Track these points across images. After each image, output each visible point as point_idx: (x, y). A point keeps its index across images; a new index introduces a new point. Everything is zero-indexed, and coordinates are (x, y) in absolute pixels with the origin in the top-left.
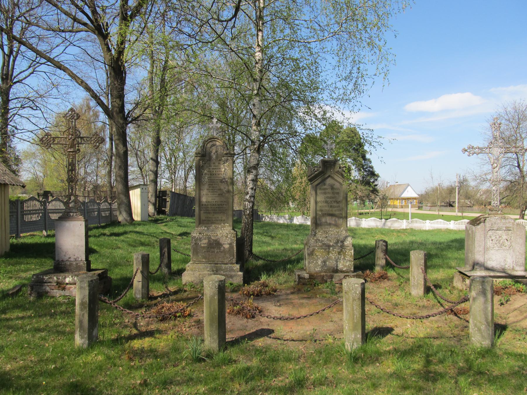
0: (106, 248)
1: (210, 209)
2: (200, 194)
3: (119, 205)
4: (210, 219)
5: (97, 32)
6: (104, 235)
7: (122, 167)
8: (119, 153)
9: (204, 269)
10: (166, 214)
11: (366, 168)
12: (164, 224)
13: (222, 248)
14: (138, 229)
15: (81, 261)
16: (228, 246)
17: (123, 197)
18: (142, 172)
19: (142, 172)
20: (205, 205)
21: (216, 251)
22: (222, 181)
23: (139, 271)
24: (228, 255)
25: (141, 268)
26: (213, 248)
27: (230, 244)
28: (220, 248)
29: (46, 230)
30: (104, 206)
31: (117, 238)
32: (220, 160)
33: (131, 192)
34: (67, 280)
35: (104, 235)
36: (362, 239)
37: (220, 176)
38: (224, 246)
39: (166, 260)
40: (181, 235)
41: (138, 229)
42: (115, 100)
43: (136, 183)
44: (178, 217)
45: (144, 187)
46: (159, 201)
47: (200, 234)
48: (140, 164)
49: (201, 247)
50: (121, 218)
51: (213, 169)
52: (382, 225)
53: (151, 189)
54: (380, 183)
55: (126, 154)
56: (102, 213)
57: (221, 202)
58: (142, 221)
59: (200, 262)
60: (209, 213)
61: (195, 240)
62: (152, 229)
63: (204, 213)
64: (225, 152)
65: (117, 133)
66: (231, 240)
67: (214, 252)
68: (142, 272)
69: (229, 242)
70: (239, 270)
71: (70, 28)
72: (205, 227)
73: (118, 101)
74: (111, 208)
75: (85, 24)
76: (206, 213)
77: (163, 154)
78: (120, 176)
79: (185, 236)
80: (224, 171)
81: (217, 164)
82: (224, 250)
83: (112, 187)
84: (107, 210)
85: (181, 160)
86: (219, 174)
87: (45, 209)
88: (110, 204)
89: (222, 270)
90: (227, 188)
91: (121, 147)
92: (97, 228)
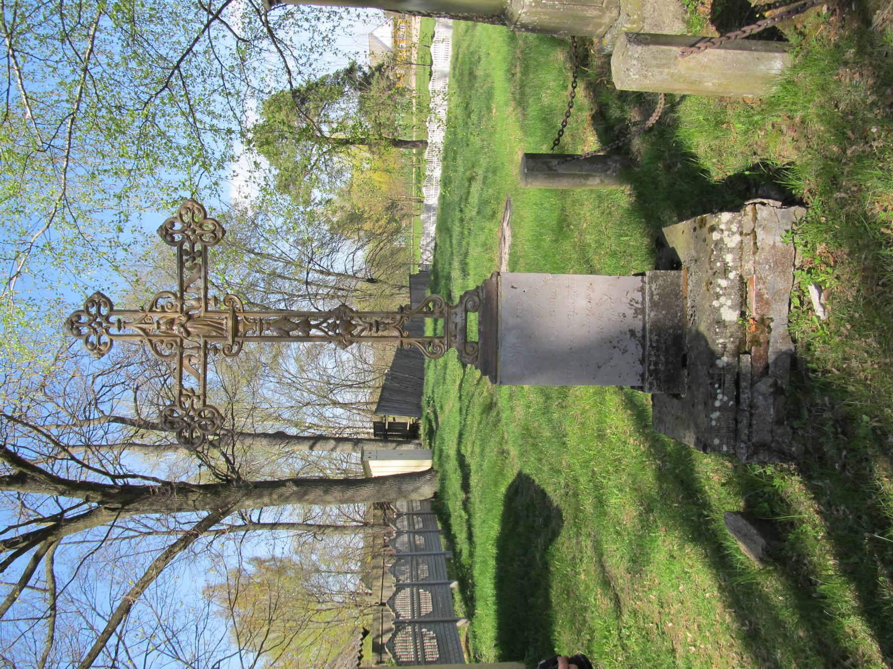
6: (466, 504)
15: (642, 290)
29: (456, 621)
30: (403, 524)
34: (730, 315)
42: (190, 502)
50: (427, 491)
54: (365, 62)
56: (416, 527)
71: (48, 595)
73: (193, 497)
75: (37, 559)
87: (412, 623)
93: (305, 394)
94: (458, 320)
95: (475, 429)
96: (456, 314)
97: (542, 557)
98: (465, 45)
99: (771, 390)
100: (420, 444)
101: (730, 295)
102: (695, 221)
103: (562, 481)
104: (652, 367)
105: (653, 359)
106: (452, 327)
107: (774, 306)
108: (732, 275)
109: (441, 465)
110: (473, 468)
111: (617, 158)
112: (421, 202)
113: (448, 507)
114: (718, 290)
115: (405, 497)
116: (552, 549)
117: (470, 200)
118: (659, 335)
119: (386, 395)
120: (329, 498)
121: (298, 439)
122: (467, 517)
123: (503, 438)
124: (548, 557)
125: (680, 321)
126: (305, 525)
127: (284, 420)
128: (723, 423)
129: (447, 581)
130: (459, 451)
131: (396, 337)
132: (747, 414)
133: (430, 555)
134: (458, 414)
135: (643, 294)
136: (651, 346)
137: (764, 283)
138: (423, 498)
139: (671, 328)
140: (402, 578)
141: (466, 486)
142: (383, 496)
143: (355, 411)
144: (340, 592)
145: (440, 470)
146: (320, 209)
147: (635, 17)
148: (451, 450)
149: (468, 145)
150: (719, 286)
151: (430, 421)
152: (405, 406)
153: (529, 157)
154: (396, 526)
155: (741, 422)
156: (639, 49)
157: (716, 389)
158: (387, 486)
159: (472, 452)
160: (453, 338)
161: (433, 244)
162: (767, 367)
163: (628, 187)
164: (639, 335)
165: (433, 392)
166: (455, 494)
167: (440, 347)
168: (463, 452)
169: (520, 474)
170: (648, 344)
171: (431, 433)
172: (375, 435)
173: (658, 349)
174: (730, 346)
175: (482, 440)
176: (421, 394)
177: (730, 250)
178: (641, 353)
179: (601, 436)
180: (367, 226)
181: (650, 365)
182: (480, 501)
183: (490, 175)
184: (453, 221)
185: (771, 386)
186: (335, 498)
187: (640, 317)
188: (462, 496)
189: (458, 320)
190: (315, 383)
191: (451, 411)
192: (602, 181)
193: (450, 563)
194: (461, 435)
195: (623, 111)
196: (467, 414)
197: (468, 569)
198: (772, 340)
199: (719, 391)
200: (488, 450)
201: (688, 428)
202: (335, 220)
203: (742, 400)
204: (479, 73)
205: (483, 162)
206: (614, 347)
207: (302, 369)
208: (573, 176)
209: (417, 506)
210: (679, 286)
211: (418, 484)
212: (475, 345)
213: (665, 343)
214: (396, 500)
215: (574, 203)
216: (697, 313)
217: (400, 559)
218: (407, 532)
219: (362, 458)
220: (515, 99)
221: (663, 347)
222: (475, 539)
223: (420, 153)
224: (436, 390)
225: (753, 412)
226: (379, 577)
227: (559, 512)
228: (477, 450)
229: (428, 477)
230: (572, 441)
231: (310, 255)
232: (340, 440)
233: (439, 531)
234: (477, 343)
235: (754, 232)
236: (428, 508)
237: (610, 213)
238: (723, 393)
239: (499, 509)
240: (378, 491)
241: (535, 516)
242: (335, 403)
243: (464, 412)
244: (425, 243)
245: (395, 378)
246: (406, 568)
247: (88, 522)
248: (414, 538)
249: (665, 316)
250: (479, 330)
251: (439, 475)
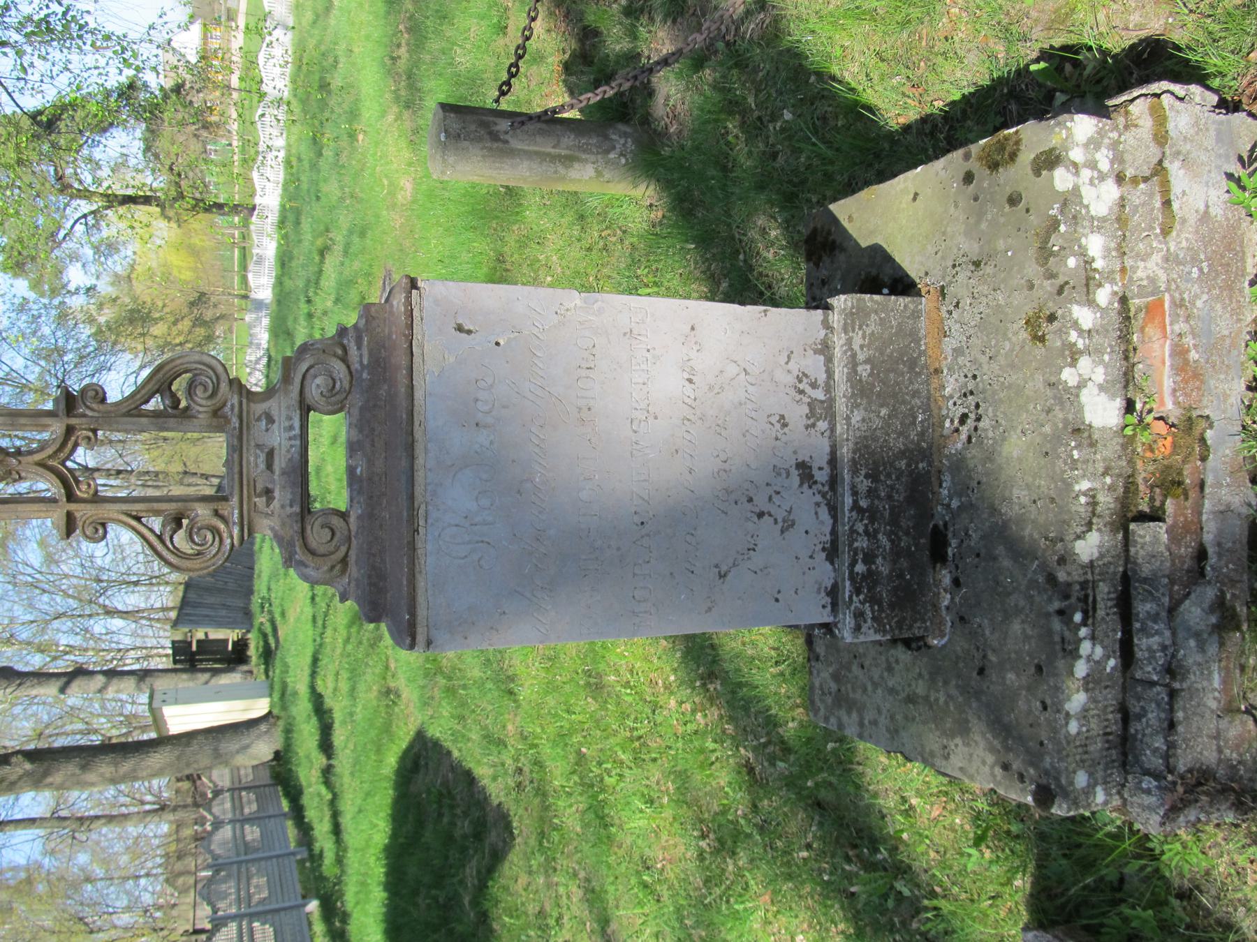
6: (327, 772)
15: (825, 349)
50: (263, 749)
56: (247, 811)
93: (58, 599)
94: (279, 438)
95: (339, 651)
96: (270, 420)
97: (475, 903)
98: (311, 43)
99: (1213, 619)
100: (251, 672)
101: (1099, 352)
102: (967, 157)
103: (509, 762)
104: (860, 568)
105: (862, 543)
106: (255, 462)
107: (1212, 383)
108: (1103, 296)
109: (284, 708)
110: (338, 716)
111: (622, 127)
112: (245, 297)
113: (298, 778)
114: (1073, 336)
115: (226, 763)
116: (494, 888)
117: (323, 283)
118: (873, 476)
119: (192, 596)
120: (91, 777)
121: (40, 676)
122: (329, 796)
123: (387, 667)
124: (487, 905)
125: (922, 434)
126: (56, 819)
127: (20, 643)
128: (1094, 724)
129: (300, 901)
130: (313, 688)
131: (53, 500)
132: (1160, 692)
133: (271, 858)
134: (309, 626)
135: (829, 360)
136: (856, 507)
137: (1188, 318)
138: (255, 762)
139: (902, 454)
140: (221, 905)
141: (326, 746)
142: (188, 765)
143: (144, 622)
144: (128, 909)
145: (282, 714)
146: (77, 302)
148: (299, 683)
149: (318, 198)
150: (1076, 325)
151: (265, 636)
152: (224, 613)
153: (445, 107)
154: (211, 813)
155: (1139, 717)
157: (1077, 627)
158: (195, 746)
159: (335, 689)
160: (260, 502)
161: (265, 360)
162: (1201, 554)
163: (651, 191)
164: (822, 476)
165: (269, 589)
166: (308, 757)
167: (215, 531)
168: (320, 688)
169: (420, 736)
170: (848, 501)
171: (268, 655)
172: (175, 662)
173: (872, 514)
174: (1106, 501)
175: (353, 671)
176: (250, 592)
177: (1098, 225)
178: (827, 529)
179: (596, 687)
180: (158, 330)
181: (853, 564)
182: (352, 774)
183: (356, 239)
184: (295, 320)
185: (1211, 610)
186: (102, 775)
187: (822, 425)
188: (321, 760)
189: (279, 438)
190: (75, 581)
191: (298, 620)
192: (599, 174)
193: (304, 867)
194: (315, 660)
195: (634, 36)
196: (324, 627)
197: (335, 884)
198: (1209, 480)
199: (1083, 632)
200: (361, 687)
201: (963, 729)
202: (102, 320)
203: (1139, 654)
204: (337, 81)
205: (344, 220)
206: (761, 515)
207: (50, 560)
208: (543, 157)
209: (248, 776)
210: (918, 341)
211: (246, 741)
212: (336, 522)
213: (890, 497)
214: (210, 768)
215: (522, 244)
216: (987, 410)
217: (217, 872)
218: (231, 821)
219: (150, 704)
220: (397, 99)
221: (885, 507)
222: (346, 837)
223: (246, 224)
224: (273, 586)
225: (1177, 685)
226: (189, 888)
227: (504, 820)
228: (344, 686)
229: (263, 727)
230: (526, 692)
231: (60, 375)
232: (112, 674)
233: (285, 815)
234: (343, 515)
235: (1159, 169)
236: (265, 776)
237: (605, 248)
238: (1093, 638)
239: (385, 796)
240: (178, 758)
241: (455, 815)
242: (110, 612)
243: (320, 623)
244: (253, 358)
246: (230, 887)
249: (887, 421)
250: (351, 471)
251: (281, 723)
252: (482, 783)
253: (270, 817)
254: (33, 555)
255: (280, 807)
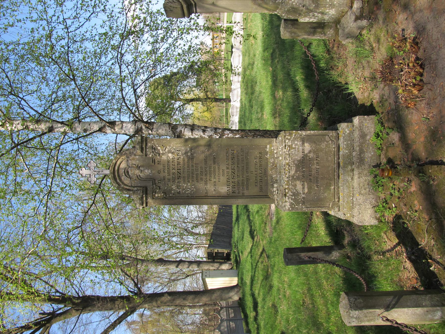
0: (275, 321)
1: (241, 178)
2: (214, 197)
3: (222, 300)
4: (259, 178)
5: (48, 325)
6: (256, 319)
7: (184, 297)
8: (170, 301)
9: (349, 187)
10: (230, 253)
11: (186, 73)
12: (240, 254)
13: (311, 155)
14: (248, 281)
16: (306, 145)
17: (214, 296)
18: (190, 275)
19: (190, 275)
20: (234, 187)
21: (315, 166)
22: (191, 158)
23: (385, 314)
24: (323, 145)
25: (378, 311)
26: (310, 171)
27: (303, 140)
28: (310, 160)
30: (224, 315)
31: (260, 305)
32: (154, 161)
33: (210, 287)
35: (256, 319)
36: (255, 56)
37: (181, 160)
38: (306, 152)
39: (320, 255)
40: (253, 237)
41: (248, 281)
42: (116, 306)
43: (201, 282)
44: (233, 240)
45: (204, 274)
46: (218, 259)
47: (285, 195)
48: (184, 277)
49: (309, 192)
51: (169, 173)
52: (238, 51)
53: (206, 267)
55: (170, 294)
56: (231, 316)
57: (227, 159)
58: (238, 276)
59: (337, 194)
60: (248, 180)
61: (298, 203)
62: (247, 266)
63: (247, 189)
64: (139, 152)
65: (150, 302)
66: (295, 139)
67: (317, 169)
68: (388, 308)
69: (299, 143)
70: (349, 124)
72: (273, 187)
73: (117, 303)
74: (225, 307)
76: (247, 184)
77: (174, 256)
78: (194, 299)
79: (254, 233)
80: (173, 153)
81: (161, 167)
82: (314, 152)
83: (205, 305)
84: (227, 311)
85: (179, 239)
86: (179, 163)
88: (222, 308)
89: (351, 154)
90: (202, 149)
91: (163, 299)
92: (247, 324)
147: (349, 215)
156: (357, 312)
233: (242, 319)
245: (218, 228)
247: (65, 316)
248: (230, 323)
252: (262, 33)
253: (238, 320)
254: (166, 214)
255: (241, 317)
